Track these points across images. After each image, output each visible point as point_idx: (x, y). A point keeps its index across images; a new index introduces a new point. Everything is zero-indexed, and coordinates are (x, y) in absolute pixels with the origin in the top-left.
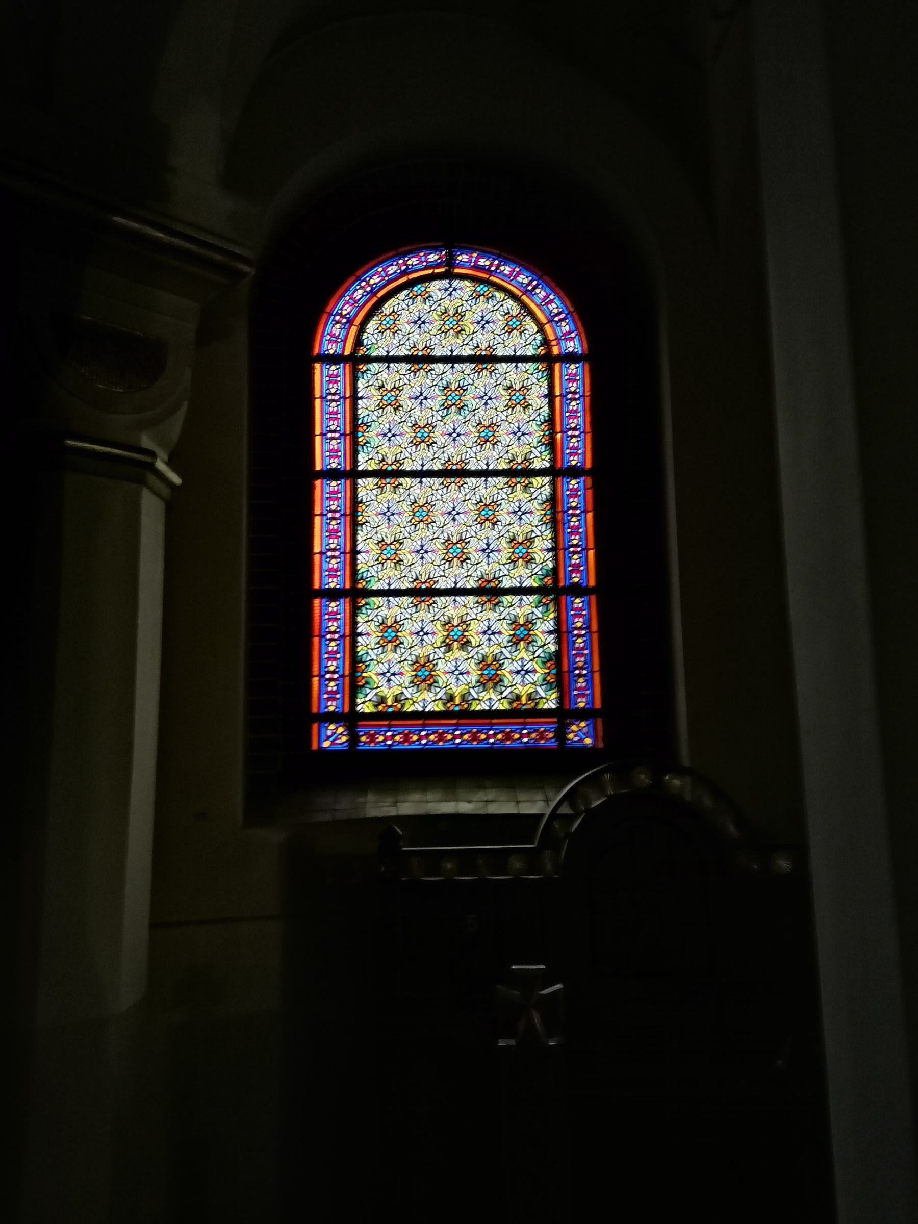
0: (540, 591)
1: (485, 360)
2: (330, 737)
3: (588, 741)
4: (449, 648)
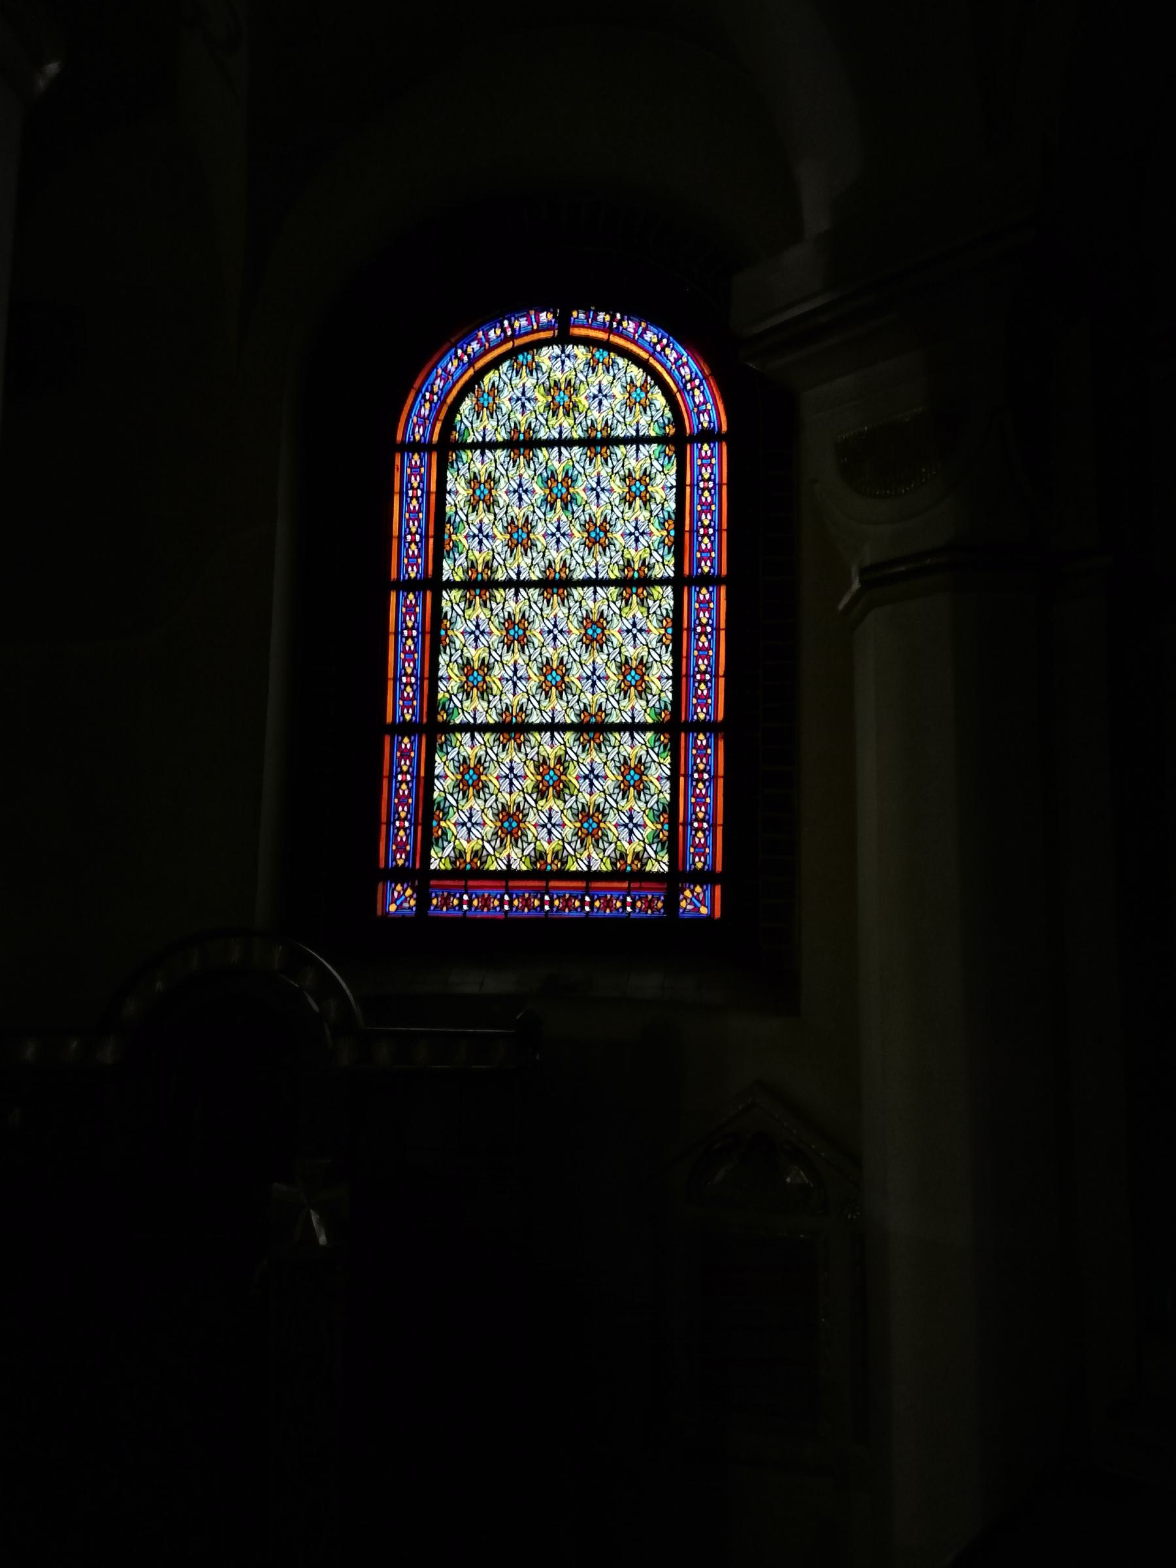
0: (657, 727)
1: (598, 443)
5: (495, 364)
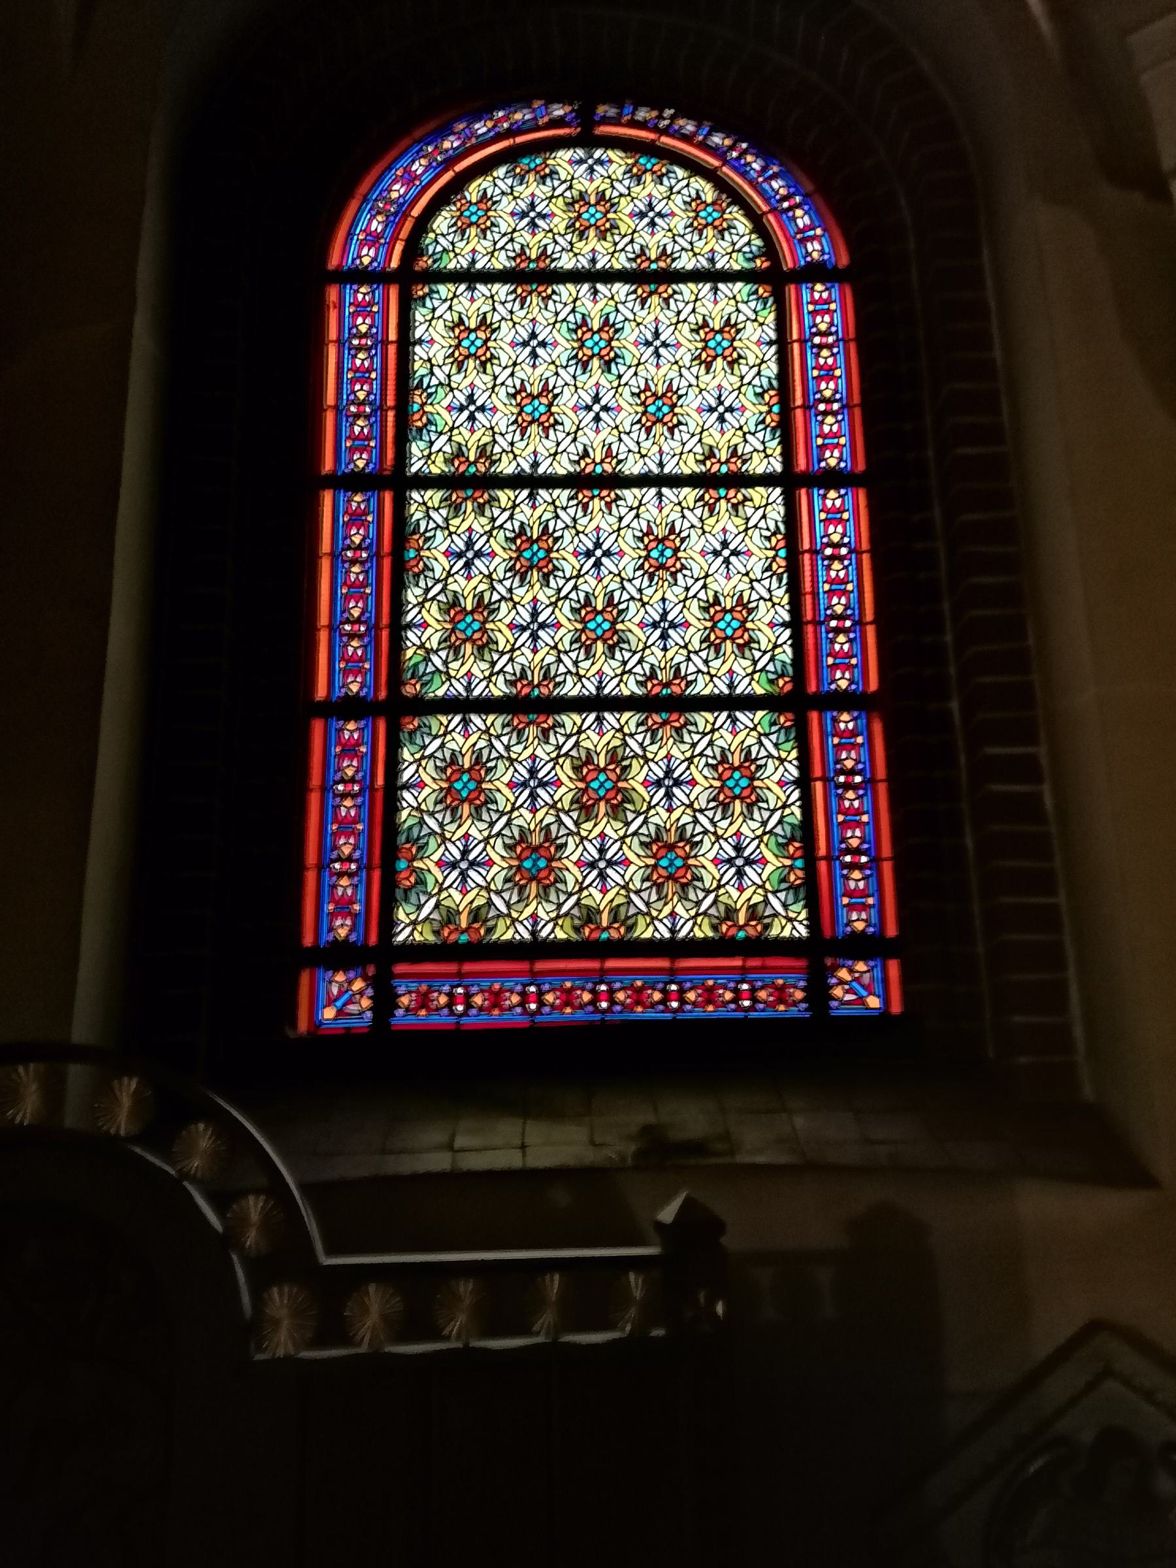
1: (652, 277)
2: (336, 1000)
3: (874, 1002)
5: (484, 168)
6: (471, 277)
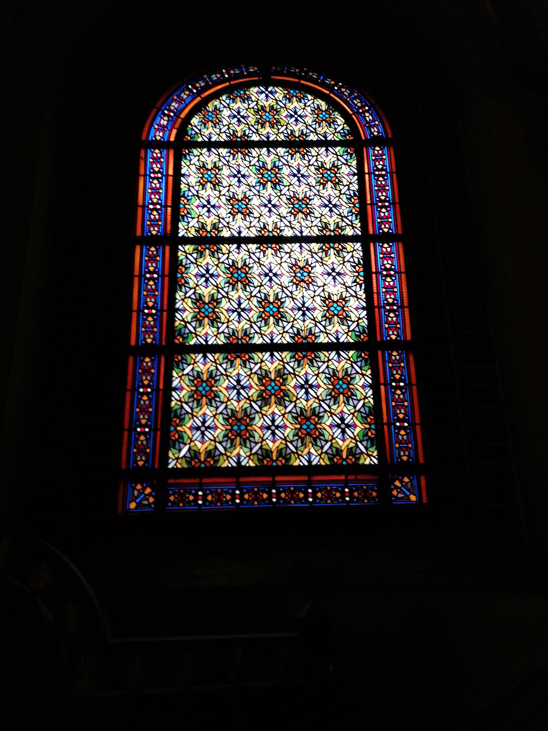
4: (279, 373)
6: (210, 145)
